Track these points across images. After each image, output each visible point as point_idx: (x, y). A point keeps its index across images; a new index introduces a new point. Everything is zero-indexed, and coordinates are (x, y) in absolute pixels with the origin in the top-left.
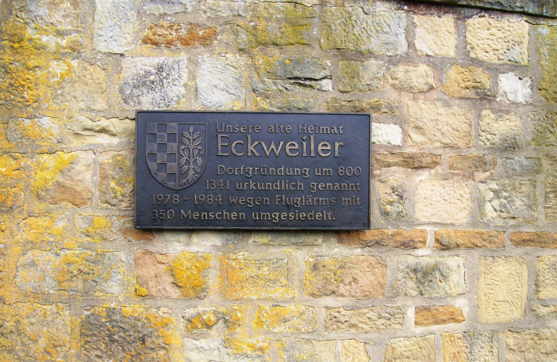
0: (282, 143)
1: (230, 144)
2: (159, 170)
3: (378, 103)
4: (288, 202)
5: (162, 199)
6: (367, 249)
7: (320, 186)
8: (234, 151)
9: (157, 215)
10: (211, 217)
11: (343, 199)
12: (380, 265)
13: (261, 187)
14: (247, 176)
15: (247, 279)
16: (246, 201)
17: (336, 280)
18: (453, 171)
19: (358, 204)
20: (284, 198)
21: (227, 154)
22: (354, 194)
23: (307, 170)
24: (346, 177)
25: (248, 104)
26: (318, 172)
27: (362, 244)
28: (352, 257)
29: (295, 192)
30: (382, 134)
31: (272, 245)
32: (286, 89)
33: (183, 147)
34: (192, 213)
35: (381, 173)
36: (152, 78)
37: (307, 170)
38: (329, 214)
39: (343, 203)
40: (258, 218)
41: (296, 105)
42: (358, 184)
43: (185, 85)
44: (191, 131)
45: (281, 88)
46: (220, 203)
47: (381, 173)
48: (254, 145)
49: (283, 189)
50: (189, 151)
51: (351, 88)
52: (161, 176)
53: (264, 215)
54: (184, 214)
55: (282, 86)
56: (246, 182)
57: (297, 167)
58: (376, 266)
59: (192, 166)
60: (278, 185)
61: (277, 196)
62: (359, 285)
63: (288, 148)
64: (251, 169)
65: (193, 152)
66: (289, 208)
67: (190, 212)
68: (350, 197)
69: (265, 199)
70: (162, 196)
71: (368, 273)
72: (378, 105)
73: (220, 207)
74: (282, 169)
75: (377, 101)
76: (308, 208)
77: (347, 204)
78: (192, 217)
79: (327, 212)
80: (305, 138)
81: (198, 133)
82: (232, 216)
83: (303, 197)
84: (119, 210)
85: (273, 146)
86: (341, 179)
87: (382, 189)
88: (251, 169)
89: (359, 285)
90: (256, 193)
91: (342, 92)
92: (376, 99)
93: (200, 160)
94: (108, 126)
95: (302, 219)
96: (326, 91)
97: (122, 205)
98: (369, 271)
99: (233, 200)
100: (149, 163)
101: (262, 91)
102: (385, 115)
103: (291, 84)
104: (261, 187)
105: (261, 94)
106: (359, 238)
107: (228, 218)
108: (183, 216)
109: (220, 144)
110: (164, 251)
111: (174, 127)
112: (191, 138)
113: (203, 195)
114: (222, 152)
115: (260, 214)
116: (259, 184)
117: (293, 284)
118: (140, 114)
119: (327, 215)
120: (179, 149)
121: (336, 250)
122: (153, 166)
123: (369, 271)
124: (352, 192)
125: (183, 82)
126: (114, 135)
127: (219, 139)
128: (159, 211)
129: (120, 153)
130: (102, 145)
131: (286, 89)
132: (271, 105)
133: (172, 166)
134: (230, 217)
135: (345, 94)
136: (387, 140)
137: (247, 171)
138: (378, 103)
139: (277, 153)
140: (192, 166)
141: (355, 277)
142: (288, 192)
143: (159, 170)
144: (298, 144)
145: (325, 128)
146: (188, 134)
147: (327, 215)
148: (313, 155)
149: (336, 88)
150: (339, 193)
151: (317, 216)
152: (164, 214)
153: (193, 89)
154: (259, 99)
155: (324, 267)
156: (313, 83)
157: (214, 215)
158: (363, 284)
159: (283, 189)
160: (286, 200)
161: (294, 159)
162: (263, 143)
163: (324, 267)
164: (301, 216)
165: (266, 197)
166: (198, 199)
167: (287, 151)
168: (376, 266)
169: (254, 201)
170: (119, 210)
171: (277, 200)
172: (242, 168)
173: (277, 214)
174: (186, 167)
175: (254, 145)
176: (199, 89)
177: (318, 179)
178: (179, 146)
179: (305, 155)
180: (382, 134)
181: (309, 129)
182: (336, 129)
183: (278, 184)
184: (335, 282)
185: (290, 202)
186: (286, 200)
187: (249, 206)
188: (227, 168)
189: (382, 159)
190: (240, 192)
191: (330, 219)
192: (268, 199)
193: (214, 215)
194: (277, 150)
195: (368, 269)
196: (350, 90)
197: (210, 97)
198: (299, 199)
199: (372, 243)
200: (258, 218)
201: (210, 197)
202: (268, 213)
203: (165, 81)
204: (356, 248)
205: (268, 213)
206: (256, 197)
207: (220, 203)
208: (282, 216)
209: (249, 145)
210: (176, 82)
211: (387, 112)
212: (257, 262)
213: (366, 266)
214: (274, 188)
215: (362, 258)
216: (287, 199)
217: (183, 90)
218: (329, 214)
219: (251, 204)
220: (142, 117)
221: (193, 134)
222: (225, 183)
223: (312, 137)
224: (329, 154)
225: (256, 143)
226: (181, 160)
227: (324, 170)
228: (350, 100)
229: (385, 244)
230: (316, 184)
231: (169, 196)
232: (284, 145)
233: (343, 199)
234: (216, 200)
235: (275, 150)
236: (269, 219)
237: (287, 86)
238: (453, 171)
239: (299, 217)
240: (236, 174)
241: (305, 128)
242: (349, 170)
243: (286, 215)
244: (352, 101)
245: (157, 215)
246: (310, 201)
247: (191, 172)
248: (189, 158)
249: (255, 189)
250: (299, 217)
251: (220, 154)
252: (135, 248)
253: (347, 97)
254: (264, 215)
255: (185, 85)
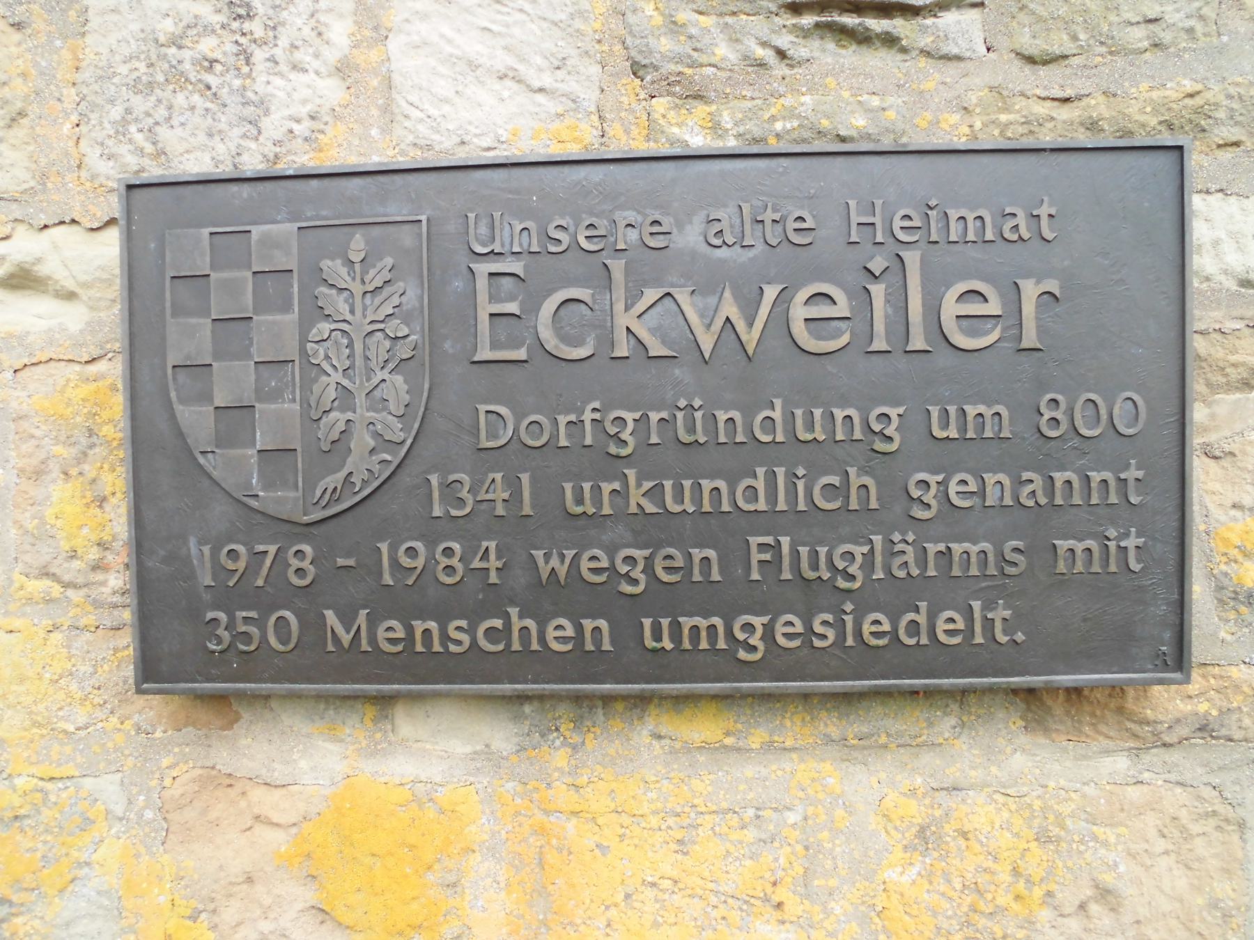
0: (771, 293)
1: (533, 307)
2: (224, 439)
3: (1198, 101)
4: (805, 564)
5: (241, 565)
6: (1155, 757)
7: (953, 488)
8: (547, 335)
9: (226, 636)
10: (459, 643)
11: (1063, 544)
12: (1212, 822)
13: (679, 498)
14: (613, 450)
15: (628, 896)
16: (612, 568)
17: (1018, 897)
18: (436, 495)
19: (1135, 566)
20: (786, 549)
21: (521, 354)
22: (1113, 522)
23: (893, 412)
24: (1076, 441)
25: (615, 130)
26: (945, 425)
27: (1136, 736)
28: (1090, 790)
29: (848, 519)
30: (1216, 243)
31: (738, 750)
32: (781, 54)
33: (325, 327)
34: (373, 622)
35: (1213, 416)
36: (207, 46)
37: (893, 412)
38: (1001, 613)
39: (1061, 567)
40: (667, 644)
41: (825, 123)
42: (1133, 474)
43: (343, 69)
44: (356, 258)
45: (760, 52)
46: (493, 578)
47: (1213, 416)
48: (641, 306)
49: (782, 506)
50: (350, 345)
51: (1075, 38)
52: (239, 467)
53: (695, 629)
54: (340, 630)
55: (764, 44)
56: (609, 479)
57: (844, 403)
58: (1196, 828)
59: (362, 413)
60: (755, 491)
61: (754, 541)
62: (1127, 919)
63: (799, 312)
64: (629, 417)
65: (366, 347)
66: (811, 593)
67: (362, 618)
68: (1093, 535)
69: (698, 554)
70: (241, 549)
71: (1164, 862)
72: (1198, 111)
73: (494, 600)
74: (777, 415)
75: (1191, 96)
76: (898, 595)
77: (1079, 567)
78: (373, 640)
79: (989, 606)
80: (877, 265)
81: (389, 261)
82: (551, 633)
83: (877, 539)
84: (98, 604)
85: (730, 309)
86: (1043, 451)
87: (1218, 487)
88: (629, 417)
89: (1127, 919)
90: (654, 529)
91: (1031, 60)
92: (1189, 86)
93: (397, 387)
94: (39, 260)
95: (874, 642)
96: (958, 58)
97: (103, 583)
98: (1166, 853)
99: (554, 562)
100: (179, 408)
101: (673, 67)
102: (1226, 155)
103: (805, 33)
104: (679, 498)
105: (669, 84)
106: (1120, 710)
107: (535, 646)
108: (336, 639)
109: (485, 308)
110: (279, 773)
111: (276, 237)
112: (357, 288)
113: (418, 545)
114: (494, 346)
115: (676, 627)
116: (668, 484)
117: (828, 913)
118: (138, 194)
119: (988, 624)
120: (303, 340)
121: (1019, 761)
122: (197, 420)
123: (1166, 853)
124: (1102, 511)
125: (332, 56)
126: (71, 296)
127: (482, 283)
128: (232, 618)
129: (92, 368)
130: (21, 338)
131: (781, 54)
132: (716, 128)
133: (277, 421)
134: (542, 639)
135: (1043, 71)
136: (1239, 269)
137: (612, 430)
138: (1198, 101)
139: (751, 338)
140: (362, 413)
141: (1108, 879)
142: (804, 520)
143: (224, 439)
144: (850, 296)
145: (970, 217)
146: (343, 271)
147: (988, 624)
148: (918, 343)
149: (1002, 43)
150: (1039, 521)
151: (941, 626)
152: (253, 630)
153: (375, 83)
154: (660, 104)
155: (964, 835)
156: (897, 25)
157: (471, 631)
158: (1143, 912)
159: (782, 506)
160: (796, 555)
161: (830, 366)
162: (683, 297)
163: (964, 835)
164: (867, 628)
165: (701, 546)
166: (395, 563)
167: (799, 329)
168: (1196, 828)
169: (649, 569)
170: (98, 604)
171: (756, 557)
172: (588, 416)
173: (758, 621)
174: (338, 418)
175: (641, 306)
176: (396, 78)
177: (946, 453)
178: (305, 326)
179: (879, 344)
180: (1216, 243)
181: (898, 223)
182: (1021, 220)
183: (760, 485)
184: (1016, 907)
185: (815, 566)
186: (796, 555)
187: (629, 589)
188: (518, 419)
189: (1219, 353)
190: (582, 526)
191: (1003, 639)
192: (711, 553)
193: (471, 631)
194: (750, 325)
195: (1161, 845)
196: (1069, 48)
197: (446, 109)
198: (860, 550)
199: (1184, 731)
200: (667, 644)
201: (448, 552)
202: (716, 621)
203: (259, 55)
204: (1107, 752)
205: (716, 621)
206: (658, 546)
207: (493, 578)
208: (780, 629)
209: (619, 307)
210: (302, 56)
211: (1236, 144)
212: (671, 821)
213: (1152, 833)
214: (741, 503)
215: (1133, 793)
216: (804, 551)
217: (331, 91)
218: (1001, 613)
219: (635, 582)
220: (149, 203)
221: (364, 272)
222: (513, 484)
223: (912, 258)
224: (994, 336)
225: (651, 295)
226: (317, 388)
227: (971, 411)
228: (1069, 92)
229: (1237, 735)
230: (933, 479)
231: (272, 549)
232: (784, 298)
233: (1063, 544)
234: (476, 564)
235: (741, 326)
236: (721, 644)
237: (784, 41)
238: (436, 495)
239: (858, 633)
240: (563, 442)
241: (877, 220)
242: (1090, 411)
243: (799, 628)
244: (1079, 98)
245: (226, 636)
246: (910, 557)
247: (362, 440)
248: (356, 386)
249: (650, 508)
250: (858, 633)
251: (485, 354)
252: (165, 762)
253: (1052, 80)
254: (695, 629)
255: (343, 69)
